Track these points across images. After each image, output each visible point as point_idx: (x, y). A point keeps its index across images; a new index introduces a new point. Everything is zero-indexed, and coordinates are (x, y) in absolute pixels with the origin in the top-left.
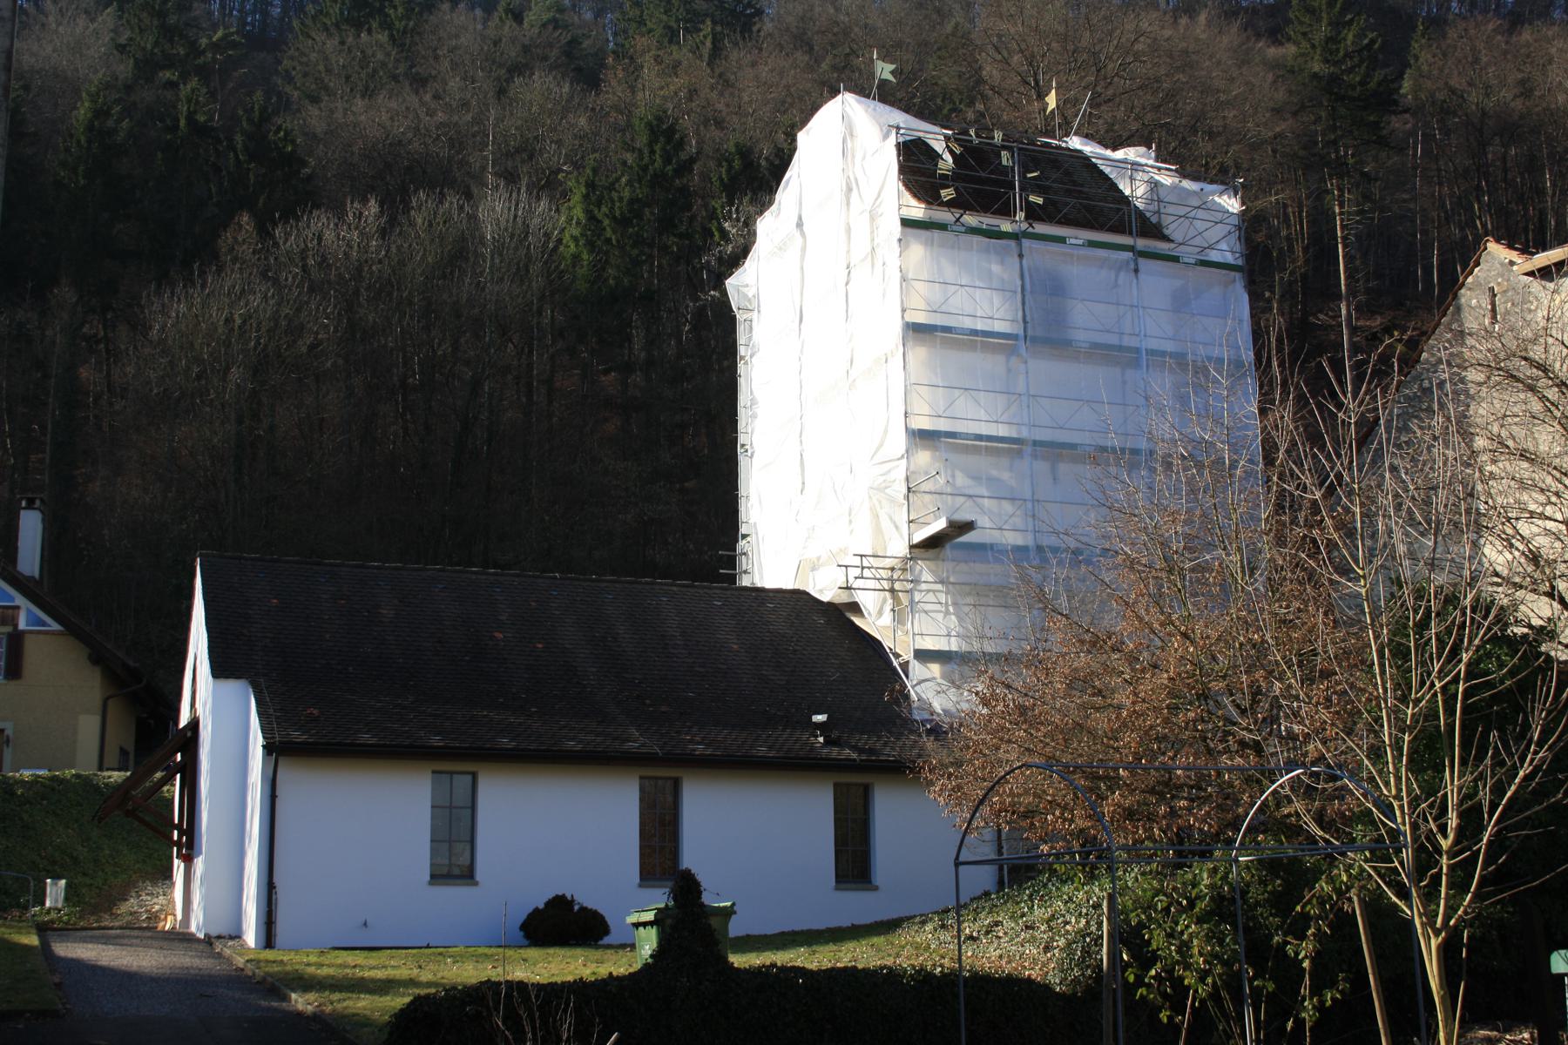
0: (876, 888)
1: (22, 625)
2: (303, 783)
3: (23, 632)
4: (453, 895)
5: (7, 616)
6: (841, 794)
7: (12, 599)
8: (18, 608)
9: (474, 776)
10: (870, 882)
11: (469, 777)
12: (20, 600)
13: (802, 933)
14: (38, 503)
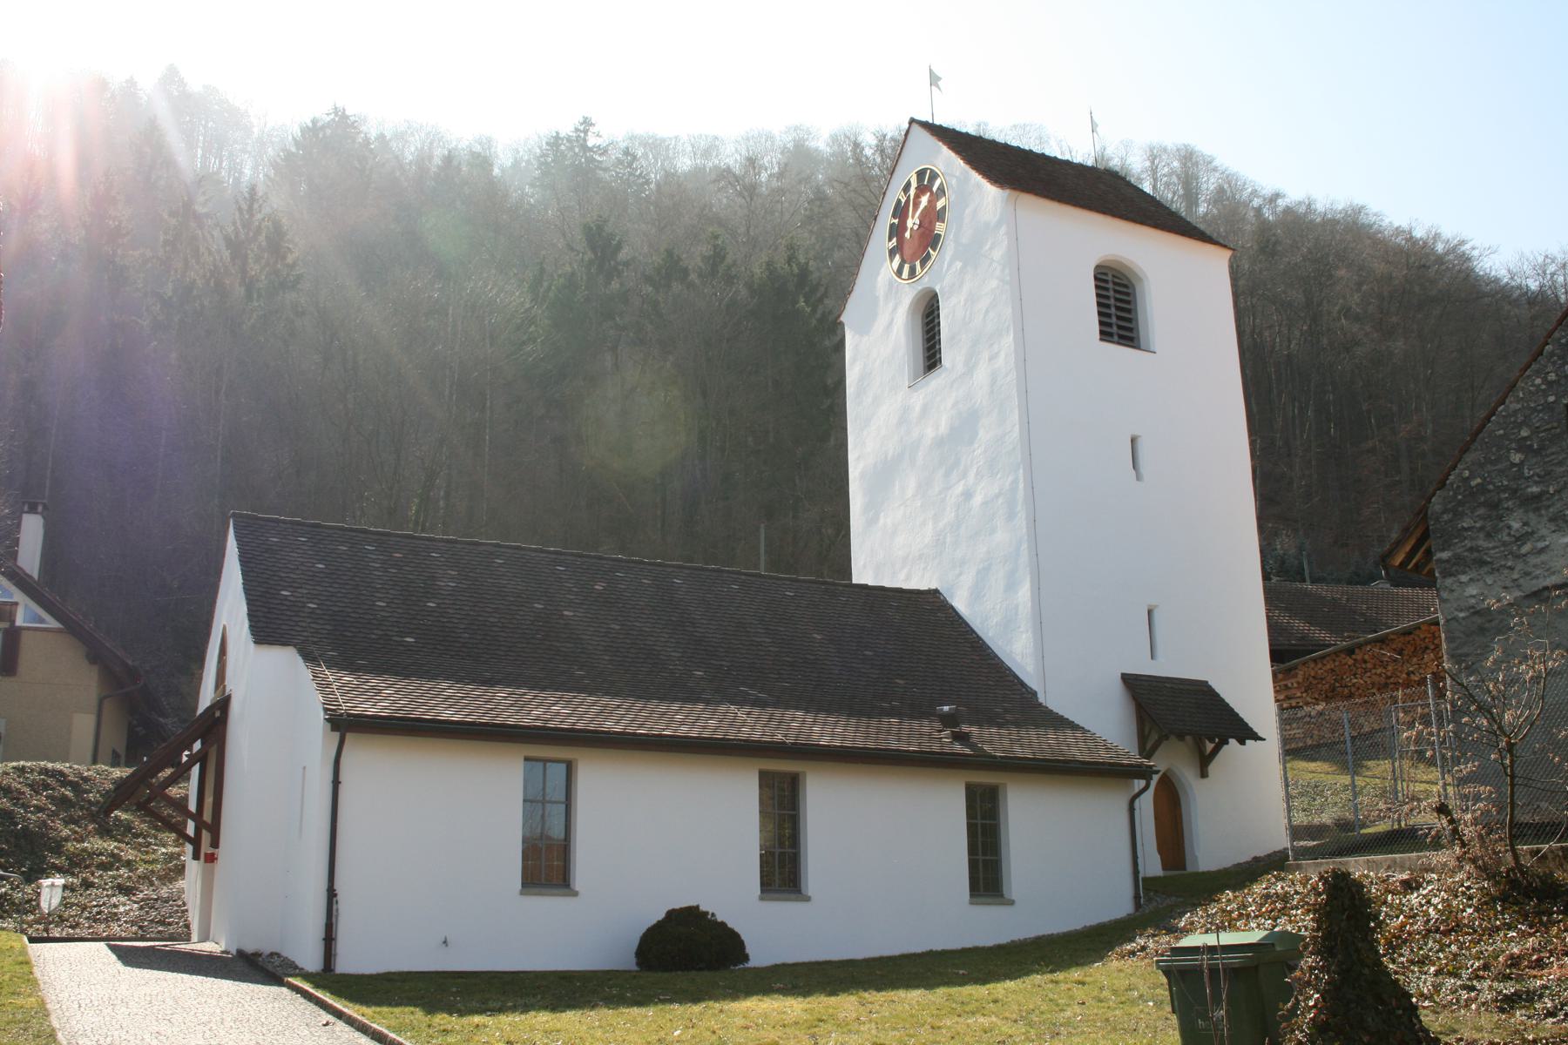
0: (576, 894)
1: (19, 622)
2: (377, 770)
3: (21, 628)
4: (548, 906)
5: (3, 612)
6: (767, 780)
7: (11, 596)
8: (16, 604)
9: (570, 767)
10: (799, 891)
11: (563, 767)
12: (18, 596)
13: (869, 962)
14: (40, 508)
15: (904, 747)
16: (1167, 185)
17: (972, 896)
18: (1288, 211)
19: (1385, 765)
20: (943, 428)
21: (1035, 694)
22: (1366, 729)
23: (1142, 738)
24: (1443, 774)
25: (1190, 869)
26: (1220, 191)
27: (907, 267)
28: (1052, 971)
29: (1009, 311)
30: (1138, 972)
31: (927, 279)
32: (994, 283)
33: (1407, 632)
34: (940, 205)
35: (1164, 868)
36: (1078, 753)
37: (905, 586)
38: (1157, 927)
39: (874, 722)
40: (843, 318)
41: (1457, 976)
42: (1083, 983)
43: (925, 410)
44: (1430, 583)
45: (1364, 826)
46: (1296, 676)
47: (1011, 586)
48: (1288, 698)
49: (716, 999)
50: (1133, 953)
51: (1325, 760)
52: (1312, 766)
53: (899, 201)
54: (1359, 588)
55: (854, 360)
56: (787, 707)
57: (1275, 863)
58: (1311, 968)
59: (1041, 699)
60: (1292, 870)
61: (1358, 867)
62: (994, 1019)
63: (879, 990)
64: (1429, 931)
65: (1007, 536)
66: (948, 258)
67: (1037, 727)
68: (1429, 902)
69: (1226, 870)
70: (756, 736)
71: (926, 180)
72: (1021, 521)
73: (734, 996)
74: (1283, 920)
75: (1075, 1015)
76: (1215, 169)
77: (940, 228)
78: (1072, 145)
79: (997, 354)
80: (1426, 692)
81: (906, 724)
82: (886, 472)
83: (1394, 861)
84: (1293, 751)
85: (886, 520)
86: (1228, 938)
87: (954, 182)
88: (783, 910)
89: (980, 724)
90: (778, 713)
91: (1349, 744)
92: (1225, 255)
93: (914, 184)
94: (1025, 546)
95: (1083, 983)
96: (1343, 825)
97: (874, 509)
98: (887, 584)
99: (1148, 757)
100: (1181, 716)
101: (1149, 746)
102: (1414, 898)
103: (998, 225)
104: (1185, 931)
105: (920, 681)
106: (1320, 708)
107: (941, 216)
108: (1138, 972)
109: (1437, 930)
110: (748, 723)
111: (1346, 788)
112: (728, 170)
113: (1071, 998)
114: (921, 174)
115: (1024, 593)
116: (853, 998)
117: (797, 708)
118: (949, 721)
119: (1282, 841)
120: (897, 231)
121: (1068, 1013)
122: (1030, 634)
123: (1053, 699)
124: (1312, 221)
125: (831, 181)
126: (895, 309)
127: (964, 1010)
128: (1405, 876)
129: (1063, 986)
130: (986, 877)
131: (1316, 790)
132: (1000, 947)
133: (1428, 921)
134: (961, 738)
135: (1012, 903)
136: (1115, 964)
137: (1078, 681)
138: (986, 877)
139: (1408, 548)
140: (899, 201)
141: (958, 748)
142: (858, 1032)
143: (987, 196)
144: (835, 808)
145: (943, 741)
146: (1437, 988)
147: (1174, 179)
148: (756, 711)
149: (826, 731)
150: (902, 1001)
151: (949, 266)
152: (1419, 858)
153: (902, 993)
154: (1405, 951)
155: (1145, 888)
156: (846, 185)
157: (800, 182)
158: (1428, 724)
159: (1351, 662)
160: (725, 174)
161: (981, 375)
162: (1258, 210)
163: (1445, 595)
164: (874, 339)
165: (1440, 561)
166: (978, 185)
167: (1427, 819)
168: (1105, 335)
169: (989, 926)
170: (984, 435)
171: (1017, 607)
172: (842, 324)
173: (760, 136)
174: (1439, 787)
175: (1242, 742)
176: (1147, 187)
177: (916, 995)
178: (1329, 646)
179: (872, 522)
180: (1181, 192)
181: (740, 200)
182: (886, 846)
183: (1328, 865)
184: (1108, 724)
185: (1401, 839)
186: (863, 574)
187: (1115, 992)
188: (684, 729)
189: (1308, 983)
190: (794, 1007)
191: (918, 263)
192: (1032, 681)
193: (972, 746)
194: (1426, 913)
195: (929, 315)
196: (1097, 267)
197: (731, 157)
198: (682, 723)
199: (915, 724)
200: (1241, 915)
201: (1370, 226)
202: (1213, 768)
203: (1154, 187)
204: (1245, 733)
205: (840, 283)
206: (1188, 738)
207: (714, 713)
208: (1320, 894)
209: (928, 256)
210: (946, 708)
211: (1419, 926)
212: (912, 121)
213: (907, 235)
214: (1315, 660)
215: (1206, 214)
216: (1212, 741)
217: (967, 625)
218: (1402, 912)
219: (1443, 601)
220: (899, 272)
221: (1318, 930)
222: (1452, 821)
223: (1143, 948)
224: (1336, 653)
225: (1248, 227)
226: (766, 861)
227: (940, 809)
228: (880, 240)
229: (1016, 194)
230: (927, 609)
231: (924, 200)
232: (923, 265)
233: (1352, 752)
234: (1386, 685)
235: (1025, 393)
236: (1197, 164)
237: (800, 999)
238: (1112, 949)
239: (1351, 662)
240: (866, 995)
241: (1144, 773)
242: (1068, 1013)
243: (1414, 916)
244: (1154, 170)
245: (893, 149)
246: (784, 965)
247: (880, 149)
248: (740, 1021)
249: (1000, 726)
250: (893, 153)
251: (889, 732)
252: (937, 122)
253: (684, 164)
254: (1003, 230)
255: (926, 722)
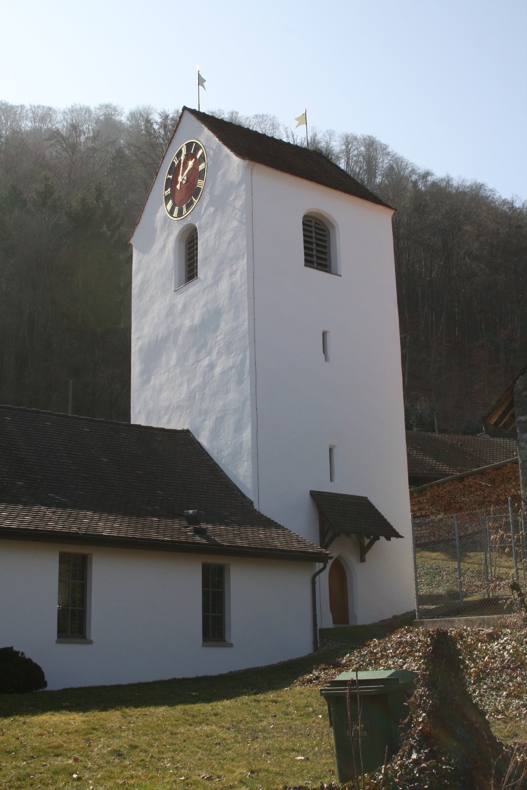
10: (84, 637)
15: (161, 538)
16: (356, 162)
17: (203, 640)
18: (434, 184)
19: (481, 555)
20: (197, 320)
21: (251, 503)
22: (470, 531)
23: (323, 534)
24: (516, 563)
25: (352, 623)
26: (391, 168)
27: (177, 209)
28: (256, 694)
29: (245, 242)
30: (313, 694)
31: (189, 217)
32: (235, 223)
33: (497, 468)
34: (201, 167)
35: (334, 623)
36: (278, 544)
37: (167, 427)
38: (328, 663)
39: (141, 520)
40: (132, 241)
41: (520, 698)
42: (276, 702)
43: (185, 307)
44: (513, 435)
45: (466, 596)
46: (426, 494)
47: (238, 429)
48: (420, 509)
49: (21, 714)
50: (310, 681)
51: (442, 551)
52: (434, 555)
53: (173, 163)
54: (470, 437)
55: (138, 271)
56: (81, 509)
57: (407, 620)
58: (421, 696)
59: (256, 507)
60: (417, 625)
61: (455, 626)
62: (214, 727)
63: (136, 707)
64: (504, 667)
65: (236, 395)
66: (205, 204)
67: (252, 526)
68: (504, 648)
69: (375, 624)
70: (59, 527)
71: (192, 150)
72: (247, 385)
73: (34, 713)
74: (410, 659)
75: (269, 724)
76: (388, 154)
77: (200, 183)
78: (291, 131)
79: (236, 271)
80: (507, 509)
81: (163, 522)
82: (156, 349)
83: (484, 620)
84: (420, 545)
85: (156, 381)
86: (363, 675)
87: (211, 152)
88: (73, 650)
89: (213, 523)
90: (74, 512)
91: (457, 542)
92: (391, 212)
93: (184, 152)
94: (248, 403)
95: (276, 702)
96: (453, 595)
97: (148, 373)
98: (154, 425)
99: (326, 548)
100: (349, 520)
101: (326, 540)
102: (495, 646)
103: (240, 184)
104: (346, 667)
105: (173, 492)
106: (440, 516)
107: (201, 175)
108: (313, 694)
109: (509, 667)
110: (54, 519)
111: (455, 570)
112: (57, 132)
113: (268, 712)
114: (189, 146)
115: (247, 435)
116: (118, 713)
117: (88, 509)
118: (192, 520)
119: (412, 605)
120: (171, 183)
121: (265, 723)
122: (250, 462)
123: (265, 507)
124: (450, 192)
125: (129, 145)
126: (167, 237)
127: (194, 721)
128: (490, 631)
129: (262, 704)
130: (214, 627)
131: (438, 571)
132: (221, 676)
133: (504, 661)
134: (201, 532)
135: (231, 645)
136: (298, 688)
137: (282, 498)
138: (214, 627)
139: (500, 413)
140: (173, 163)
141: (198, 539)
142: (120, 737)
143: (234, 163)
144: (112, 581)
145: (188, 534)
146: (507, 706)
147: (361, 159)
148: (59, 511)
149: (107, 526)
150: (152, 715)
151: (204, 213)
152: (499, 618)
153: (152, 709)
154: (488, 681)
155: (321, 636)
156: (139, 148)
157: (107, 144)
158: (507, 530)
159: (461, 486)
160: (55, 134)
161: (224, 285)
162: (415, 183)
163: (522, 444)
164: (152, 259)
165: (520, 422)
166: (228, 156)
167: (504, 591)
168: (309, 263)
169: (216, 662)
170: (224, 326)
171: (242, 443)
172: (130, 246)
173: (81, 109)
174: (513, 571)
175: (388, 539)
176: (342, 165)
177: (162, 710)
178: (449, 475)
179: (146, 382)
180: (365, 168)
181: (65, 154)
182: (145, 605)
183: (432, 626)
184: (299, 524)
185: (490, 605)
186: (139, 417)
187: (297, 708)
188: (8, 522)
189: (419, 706)
190: (76, 719)
191: (184, 207)
192: (251, 496)
193: (208, 538)
194: (502, 656)
195: (190, 241)
196: (305, 217)
197: (60, 123)
198: (6, 518)
199: (169, 522)
200: (382, 656)
201: (487, 198)
202: (369, 555)
203: (348, 164)
204: (391, 533)
205: (130, 216)
206: (353, 536)
207: (30, 511)
208: (428, 646)
209: (192, 203)
210: (191, 512)
211: (497, 664)
212: (185, 108)
213: (178, 187)
214: (438, 485)
215: (381, 183)
216: (368, 537)
217: (208, 454)
218: (487, 654)
219: (521, 448)
220: (171, 212)
221: (426, 670)
222: (520, 595)
223: (317, 678)
224: (452, 480)
225: (408, 194)
226: (62, 615)
227: (185, 582)
228: (160, 189)
229: (253, 163)
230: (183, 441)
231: (191, 163)
232: (188, 209)
233: (458, 546)
234: (483, 502)
235: (253, 298)
236: (376, 149)
237: (81, 714)
238: (296, 678)
239: (461, 486)
240: (127, 710)
241: (323, 558)
242: (265, 723)
243: (494, 658)
244: (348, 152)
245: (173, 125)
246: (72, 689)
247: (164, 125)
248: (37, 730)
249: (227, 525)
250: (173, 126)
251: (151, 527)
252: (202, 111)
253: (27, 125)
254: (243, 187)
255: (177, 521)
